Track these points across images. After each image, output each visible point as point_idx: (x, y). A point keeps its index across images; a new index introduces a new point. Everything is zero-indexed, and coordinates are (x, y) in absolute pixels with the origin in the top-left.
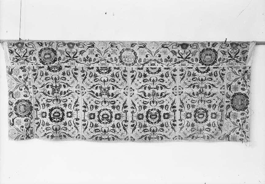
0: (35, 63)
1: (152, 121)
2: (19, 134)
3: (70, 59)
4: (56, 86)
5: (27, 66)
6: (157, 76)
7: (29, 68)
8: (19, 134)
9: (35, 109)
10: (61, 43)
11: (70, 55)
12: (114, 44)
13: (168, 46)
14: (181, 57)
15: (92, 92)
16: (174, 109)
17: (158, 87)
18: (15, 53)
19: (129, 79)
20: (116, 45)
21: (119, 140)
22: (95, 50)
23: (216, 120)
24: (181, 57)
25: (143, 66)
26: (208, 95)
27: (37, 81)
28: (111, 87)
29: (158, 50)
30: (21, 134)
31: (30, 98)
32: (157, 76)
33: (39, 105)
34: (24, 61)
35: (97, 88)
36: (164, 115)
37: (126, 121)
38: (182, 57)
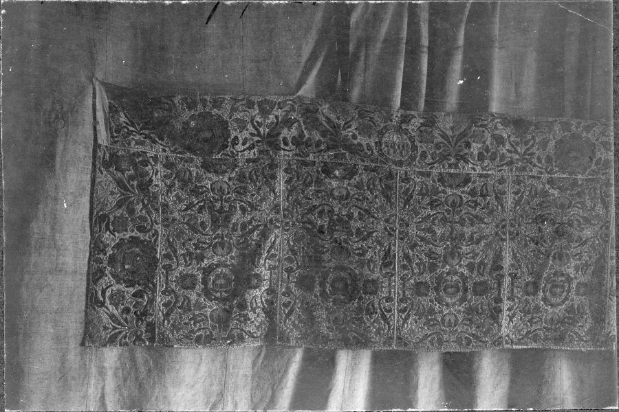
0: (172, 149)
1: (449, 300)
2: (117, 331)
3: (258, 141)
4: (221, 211)
5: (151, 153)
6: (462, 192)
7: (155, 158)
8: (117, 331)
9: (164, 267)
10: (244, 102)
11: (261, 129)
12: (365, 111)
13: (485, 123)
14: (256, 132)
15: (310, 222)
16: (497, 273)
17: (464, 219)
18: (250, 127)
19: (398, 199)
20: (371, 115)
21: (291, 350)
22: (436, 133)
23: (484, 299)
24: (256, 132)
25: (431, 168)
26: (576, 242)
27: (174, 193)
28: (356, 215)
29: (350, 121)
30: (120, 332)
31: (153, 235)
32: (462, 192)
33: (176, 257)
34: (144, 138)
35: (321, 213)
36: (195, 284)
37: (389, 299)
38: (516, 152)
